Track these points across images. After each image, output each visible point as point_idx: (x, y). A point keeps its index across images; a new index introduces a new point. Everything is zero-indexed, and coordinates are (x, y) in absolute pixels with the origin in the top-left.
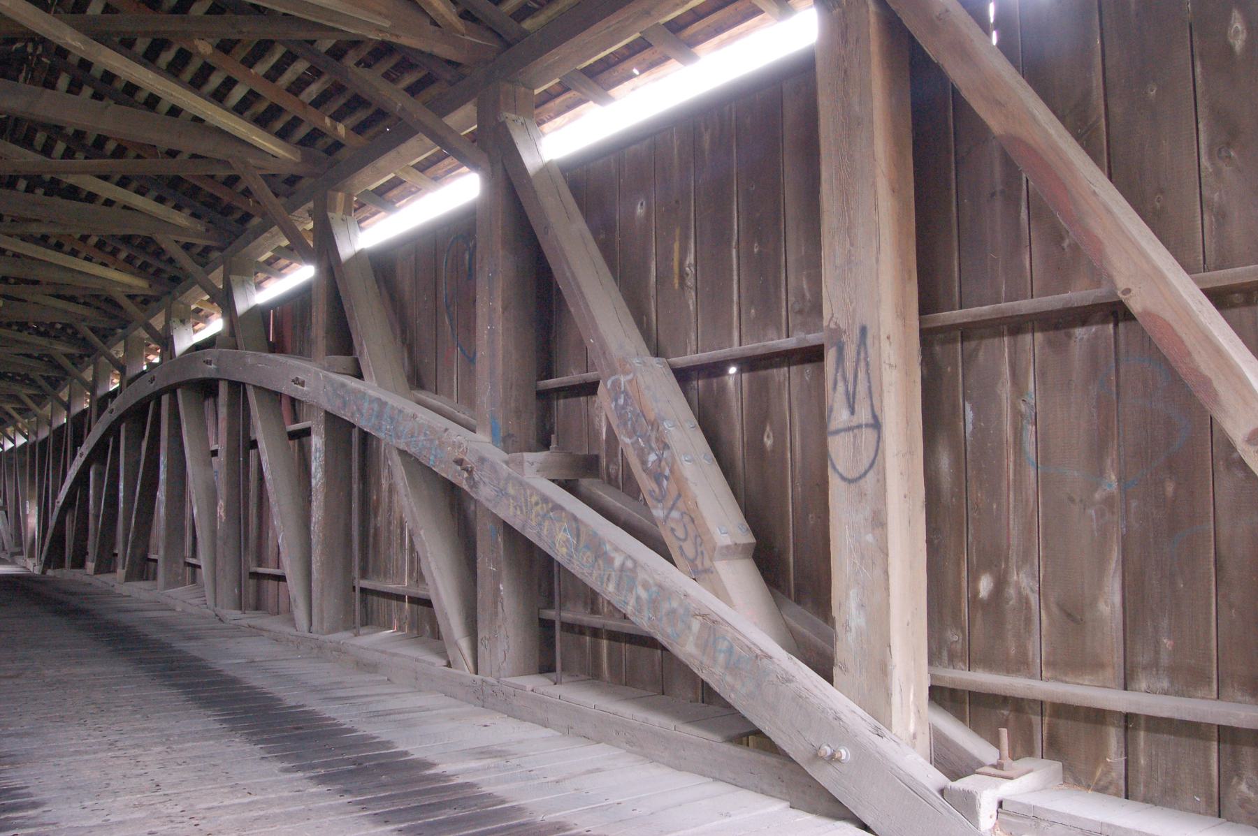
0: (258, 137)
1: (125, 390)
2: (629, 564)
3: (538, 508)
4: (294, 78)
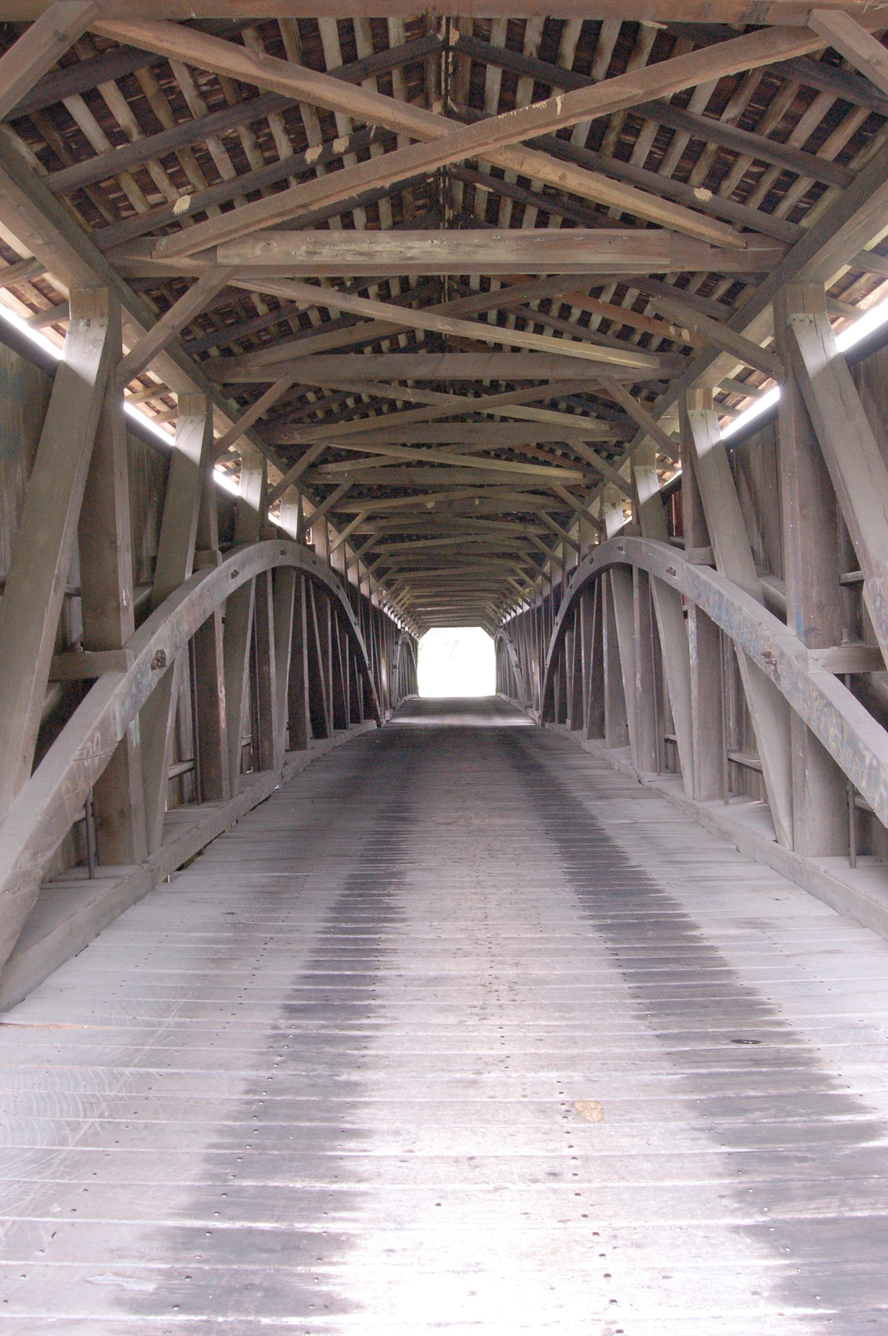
0: (615, 356)
1: (581, 564)
2: (875, 763)
3: (818, 702)
4: (634, 300)
